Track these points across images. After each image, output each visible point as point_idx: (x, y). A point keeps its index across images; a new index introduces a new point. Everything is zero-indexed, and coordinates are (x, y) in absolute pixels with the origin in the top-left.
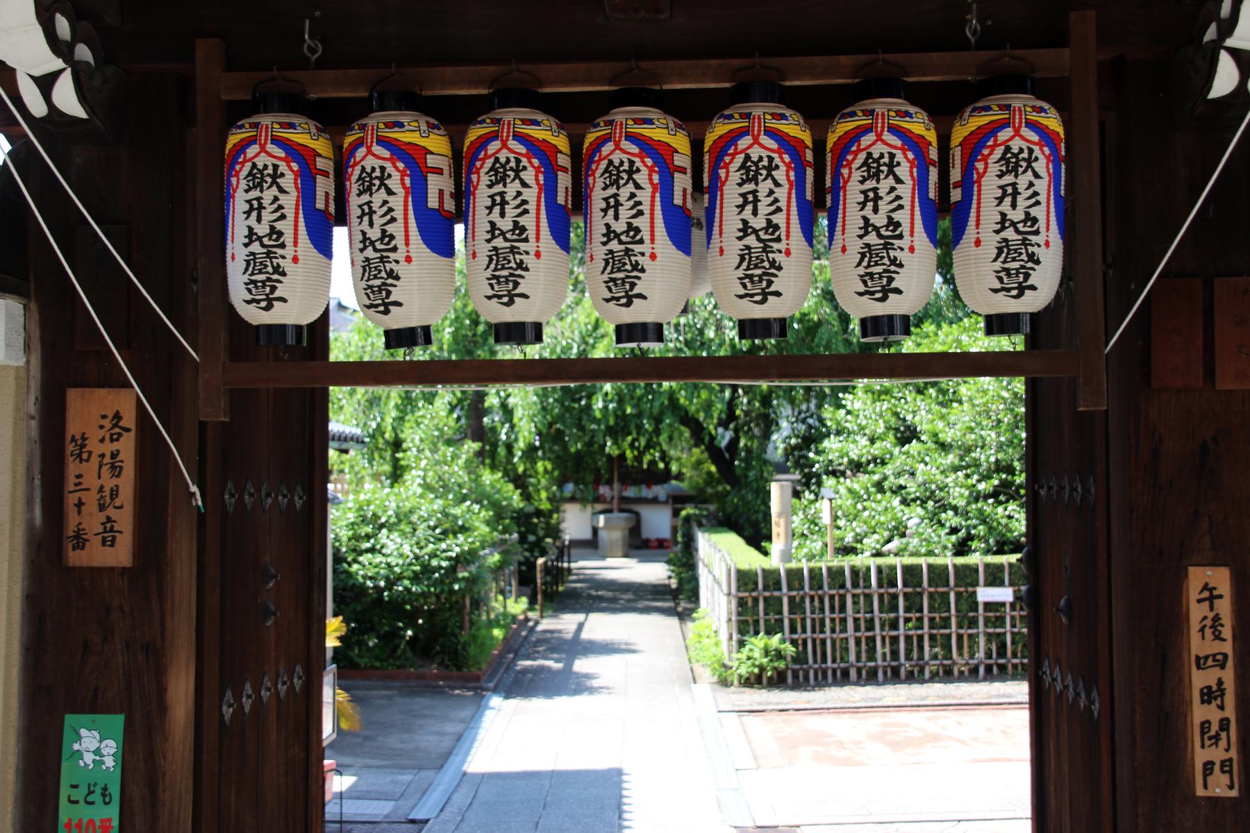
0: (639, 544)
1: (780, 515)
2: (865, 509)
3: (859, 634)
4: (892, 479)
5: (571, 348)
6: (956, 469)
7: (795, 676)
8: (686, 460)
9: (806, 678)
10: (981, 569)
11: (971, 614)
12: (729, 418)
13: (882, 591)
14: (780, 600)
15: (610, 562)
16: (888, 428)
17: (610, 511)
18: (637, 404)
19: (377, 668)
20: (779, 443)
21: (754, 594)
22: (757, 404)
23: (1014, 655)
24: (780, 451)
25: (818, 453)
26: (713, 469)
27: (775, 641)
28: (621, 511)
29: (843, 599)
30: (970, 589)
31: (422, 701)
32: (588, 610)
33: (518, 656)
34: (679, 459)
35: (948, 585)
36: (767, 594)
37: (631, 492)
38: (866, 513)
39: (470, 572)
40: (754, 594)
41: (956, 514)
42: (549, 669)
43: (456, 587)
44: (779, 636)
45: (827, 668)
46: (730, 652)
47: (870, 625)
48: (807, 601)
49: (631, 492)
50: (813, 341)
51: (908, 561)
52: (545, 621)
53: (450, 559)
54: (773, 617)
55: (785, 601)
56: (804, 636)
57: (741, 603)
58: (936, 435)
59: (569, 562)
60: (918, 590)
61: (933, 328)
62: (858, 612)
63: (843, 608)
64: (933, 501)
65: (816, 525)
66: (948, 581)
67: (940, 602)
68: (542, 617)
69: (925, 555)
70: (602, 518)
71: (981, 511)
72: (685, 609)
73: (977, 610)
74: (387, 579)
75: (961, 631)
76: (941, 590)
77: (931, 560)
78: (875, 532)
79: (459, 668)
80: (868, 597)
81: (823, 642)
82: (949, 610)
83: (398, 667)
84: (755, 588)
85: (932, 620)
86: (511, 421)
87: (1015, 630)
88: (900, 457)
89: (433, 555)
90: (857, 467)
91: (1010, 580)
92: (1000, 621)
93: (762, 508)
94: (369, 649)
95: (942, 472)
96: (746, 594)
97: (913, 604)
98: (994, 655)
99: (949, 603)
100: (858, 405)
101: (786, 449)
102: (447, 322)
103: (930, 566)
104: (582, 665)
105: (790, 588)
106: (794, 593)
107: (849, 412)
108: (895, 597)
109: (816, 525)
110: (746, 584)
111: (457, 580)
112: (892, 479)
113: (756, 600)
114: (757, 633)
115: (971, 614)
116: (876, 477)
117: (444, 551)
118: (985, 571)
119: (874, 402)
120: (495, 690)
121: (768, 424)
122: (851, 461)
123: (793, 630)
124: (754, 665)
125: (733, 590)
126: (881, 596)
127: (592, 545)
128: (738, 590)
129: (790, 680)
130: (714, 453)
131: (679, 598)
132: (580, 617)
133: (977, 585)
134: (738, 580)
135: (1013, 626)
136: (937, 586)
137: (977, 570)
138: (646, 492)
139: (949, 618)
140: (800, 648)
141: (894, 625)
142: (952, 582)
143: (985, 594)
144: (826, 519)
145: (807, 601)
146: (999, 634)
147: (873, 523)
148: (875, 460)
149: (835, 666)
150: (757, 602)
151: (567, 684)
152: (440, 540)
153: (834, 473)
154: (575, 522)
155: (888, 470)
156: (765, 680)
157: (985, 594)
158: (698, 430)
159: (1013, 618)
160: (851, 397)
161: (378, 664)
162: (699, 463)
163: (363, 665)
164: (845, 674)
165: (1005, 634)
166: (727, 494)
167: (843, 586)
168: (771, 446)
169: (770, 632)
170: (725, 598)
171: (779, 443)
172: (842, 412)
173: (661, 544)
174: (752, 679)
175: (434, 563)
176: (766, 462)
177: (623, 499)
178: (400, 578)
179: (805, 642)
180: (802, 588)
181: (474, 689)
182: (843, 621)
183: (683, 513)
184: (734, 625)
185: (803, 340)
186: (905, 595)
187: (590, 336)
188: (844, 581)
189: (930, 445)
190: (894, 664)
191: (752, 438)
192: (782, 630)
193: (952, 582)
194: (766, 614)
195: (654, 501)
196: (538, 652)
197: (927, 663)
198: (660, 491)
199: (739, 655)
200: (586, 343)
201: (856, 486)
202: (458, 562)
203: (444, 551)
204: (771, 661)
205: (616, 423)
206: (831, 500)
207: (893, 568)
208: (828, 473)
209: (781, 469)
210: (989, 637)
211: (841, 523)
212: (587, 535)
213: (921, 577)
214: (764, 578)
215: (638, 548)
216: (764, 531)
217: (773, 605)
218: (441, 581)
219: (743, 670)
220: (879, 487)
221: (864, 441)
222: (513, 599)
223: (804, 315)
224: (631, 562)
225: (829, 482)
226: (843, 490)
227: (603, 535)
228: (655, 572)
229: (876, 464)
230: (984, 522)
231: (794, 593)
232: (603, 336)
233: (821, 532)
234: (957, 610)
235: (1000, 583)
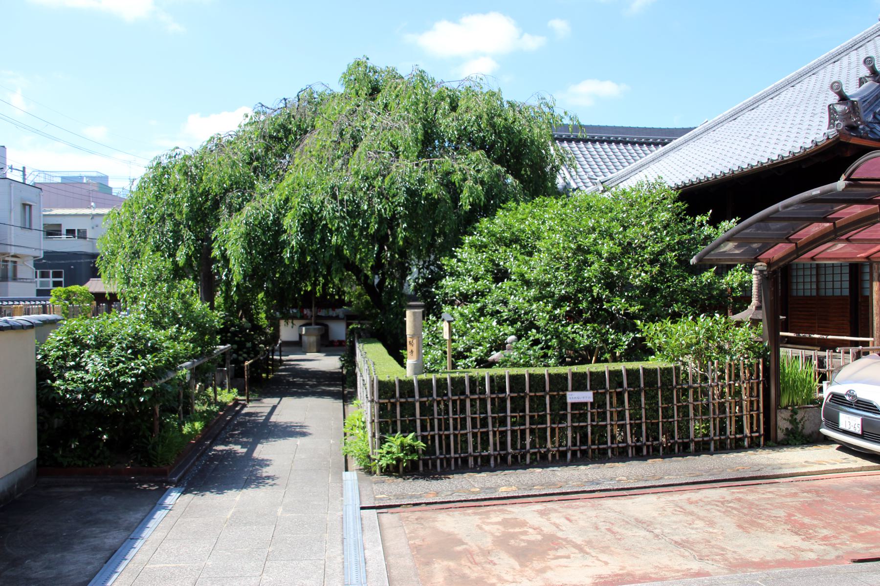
0: (326, 345)
1: (413, 337)
2: (472, 327)
4: (490, 306)
5: (269, 216)
6: (537, 299)
7: (425, 464)
8: (353, 291)
9: (434, 466)
10: (569, 377)
11: (562, 412)
12: (378, 266)
13: (494, 396)
14: (413, 405)
15: (309, 356)
16: (487, 271)
17: (310, 324)
18: (313, 253)
19: (79, 466)
20: (410, 283)
21: (392, 400)
22: (397, 256)
23: (593, 443)
24: (412, 287)
25: (437, 288)
26: (368, 298)
27: (409, 439)
28: (317, 324)
29: (463, 402)
30: (561, 393)
32: (281, 395)
33: (215, 442)
34: (349, 293)
35: (544, 390)
36: (403, 400)
37: (323, 313)
38: (474, 331)
39: (155, 387)
40: (392, 400)
41: (538, 332)
42: (235, 453)
43: (142, 400)
44: (411, 435)
45: (451, 458)
46: (373, 448)
47: (484, 423)
49: (323, 313)
50: (434, 213)
51: (515, 371)
52: (250, 404)
53: (136, 376)
54: (407, 419)
55: (417, 405)
56: (432, 433)
57: (382, 408)
58: (522, 275)
59: (280, 356)
60: (522, 394)
61: (514, 204)
62: (475, 413)
63: (463, 410)
64: (524, 325)
68: (249, 401)
69: (524, 366)
70: (304, 328)
71: (556, 329)
72: (349, 392)
73: (566, 409)
74: (84, 392)
75: (554, 426)
76: (582, 424)
77: (531, 370)
78: (480, 345)
79: (150, 465)
80: (483, 401)
81: (448, 437)
82: (545, 410)
83: (97, 465)
84: (394, 396)
85: (531, 417)
86: (227, 267)
87: (594, 423)
88: (497, 292)
89: (121, 373)
90: (465, 298)
91: (591, 385)
92: (582, 417)
93: (400, 325)
94: (72, 450)
95: (528, 301)
96: (387, 401)
97: (518, 406)
98: (578, 444)
99: (545, 404)
100: (465, 255)
101: (415, 286)
102: (185, 199)
103: (530, 375)
104: (263, 451)
105: (421, 396)
106: (425, 399)
107: (459, 261)
108: (503, 400)
109: (438, 338)
110: (386, 393)
111: (143, 394)
112: (490, 306)
113: (394, 405)
114: (395, 432)
115: (562, 412)
116: (479, 305)
117: (132, 369)
118: (572, 379)
119: (477, 253)
120: (177, 485)
121: (405, 271)
122: (461, 294)
123: (424, 428)
124: (392, 459)
125: (376, 399)
126: (493, 400)
127: (297, 345)
128: (380, 398)
129: (421, 469)
130: (369, 288)
131: (342, 385)
132: (275, 401)
133: (567, 390)
134: (379, 390)
135: (593, 420)
136: (536, 391)
137: (566, 378)
138: (332, 313)
139: (545, 416)
140: (429, 442)
141: (503, 422)
142: (547, 388)
143: (573, 397)
144: (446, 336)
146: (582, 427)
147: (478, 337)
148: (477, 293)
149: (457, 456)
150: (396, 407)
151: (239, 474)
152: (130, 359)
153: (452, 303)
154: (288, 332)
155: (489, 299)
156: (401, 469)
157: (573, 397)
158: (357, 271)
159: (592, 414)
160: (460, 250)
161: (80, 463)
162: (360, 295)
164: (465, 461)
165: (587, 426)
167: (463, 393)
168: (406, 284)
169: (405, 431)
170: (369, 404)
171: (410, 283)
173: (341, 343)
175: (122, 379)
176: (403, 295)
177: (318, 317)
178: (95, 391)
179: (433, 437)
180: (432, 395)
182: (464, 420)
183: (351, 327)
184: (376, 425)
185: (428, 212)
186: (512, 398)
187: (282, 208)
189: (519, 282)
190: (502, 452)
191: (393, 280)
192: (415, 430)
193: (547, 388)
194: (402, 416)
195: (337, 318)
196: (232, 436)
197: (528, 451)
198: (339, 312)
199: (381, 451)
200: (280, 213)
201: (466, 311)
202: (143, 378)
203: (132, 369)
204: (406, 454)
205: (299, 267)
206: (449, 322)
207: (502, 378)
208: (445, 302)
209: (413, 298)
210: (574, 429)
211: (456, 337)
212: (296, 338)
213: (524, 385)
214: (400, 387)
215: (327, 346)
216: (402, 341)
217: (407, 409)
218: (129, 395)
219: (384, 463)
220: (481, 310)
221: (470, 280)
222: (227, 390)
223: (428, 195)
224: (320, 356)
225: (447, 309)
226: (457, 315)
227: (305, 338)
228: (330, 363)
229: (478, 296)
230: (557, 337)
231: (425, 399)
232: (291, 208)
233: (442, 343)
235: (584, 389)
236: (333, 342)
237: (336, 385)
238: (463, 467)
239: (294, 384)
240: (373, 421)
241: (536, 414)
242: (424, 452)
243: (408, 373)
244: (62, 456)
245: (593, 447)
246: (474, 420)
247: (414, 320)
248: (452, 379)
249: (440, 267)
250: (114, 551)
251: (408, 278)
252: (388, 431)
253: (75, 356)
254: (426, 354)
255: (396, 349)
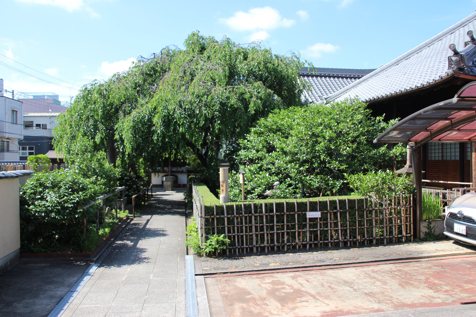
0: (176, 187)
1: (223, 182)
2: (255, 177)
3: (257, 233)
4: (265, 166)
5: (145, 117)
6: (290, 162)
7: (230, 251)
8: (191, 157)
9: (235, 252)
10: (308, 204)
12: (204, 144)
13: (267, 214)
14: (223, 219)
15: (167, 192)
16: (263, 147)
17: (168, 175)
18: (170, 137)
20: (222, 153)
21: (212, 217)
22: (215, 138)
23: (321, 240)
24: (223, 155)
25: (236, 156)
26: (199, 161)
27: (221, 237)
28: (171, 175)
29: (250, 218)
30: (304, 213)
31: (58, 270)
32: (152, 213)
33: (116, 239)
34: (189, 158)
35: (294, 211)
36: (218, 216)
37: (174, 169)
38: (256, 179)
39: (84, 209)
40: (212, 217)
41: (291, 180)
42: (127, 245)
43: (77, 216)
44: (223, 235)
45: (244, 248)
46: (202, 242)
47: (262, 229)
48: (235, 219)
49: (174, 169)
50: (235, 115)
51: (279, 201)
52: (135, 219)
53: (73, 203)
54: (220, 226)
55: (226, 219)
56: (234, 234)
57: (207, 220)
58: (282, 149)
59: (152, 192)
60: (282, 213)
61: (278, 111)
62: (257, 224)
63: (251, 222)
64: (283, 176)
65: (237, 183)
66: (294, 209)
67: (291, 218)
68: (134, 217)
70: (164, 178)
71: (301, 178)
72: (189, 212)
73: (306, 221)
74: (45, 212)
75: (299, 230)
77: (287, 200)
78: (260, 187)
79: (81, 251)
80: (261, 217)
81: (242, 236)
82: (295, 222)
83: (52, 251)
84: (213, 214)
85: (287, 226)
86: (123, 144)
87: (321, 229)
88: (269, 158)
89: (66, 202)
90: (252, 161)
91: (320, 208)
92: (315, 225)
93: (217, 176)
94: (39, 244)
95: (286, 163)
96: (209, 217)
97: (280, 219)
98: (313, 240)
99: (295, 219)
100: (251, 138)
101: (224, 155)
102: (100, 108)
103: (287, 203)
104: (142, 244)
105: (228, 214)
106: (230, 216)
107: (248, 141)
108: (272, 217)
109: (237, 183)
110: (209, 212)
111: (77, 213)
112: (265, 166)
113: (213, 219)
114: (214, 233)
116: (259, 165)
117: (72, 200)
120: (96, 262)
121: (219, 147)
122: (249, 159)
123: (229, 232)
124: (212, 248)
125: (203, 216)
126: (266, 216)
127: (161, 187)
128: (205, 215)
130: (199, 156)
131: (185, 208)
132: (149, 217)
133: (307, 211)
134: (205, 211)
135: (321, 227)
136: (290, 212)
137: (306, 205)
138: (179, 169)
139: (295, 225)
140: (232, 239)
141: (272, 228)
142: (296, 210)
143: (310, 215)
144: (241, 182)
145: (235, 219)
146: (315, 231)
147: (259, 182)
148: (258, 159)
149: (247, 246)
150: (214, 220)
151: (129, 256)
152: (71, 194)
153: (244, 164)
154: (156, 179)
155: (264, 162)
156: (217, 254)
157: (310, 215)
158: (193, 146)
159: (320, 224)
160: (249, 135)
161: (43, 250)
162: (195, 160)
163: (35, 251)
166: (204, 170)
167: (251, 213)
168: (220, 154)
169: (219, 233)
170: (200, 218)
171: (222, 153)
172: (246, 141)
173: (184, 186)
174: (212, 253)
175: (66, 205)
176: (218, 159)
178: (52, 211)
179: (234, 236)
180: (233, 214)
181: (86, 261)
182: (251, 227)
183: (190, 177)
184: (203, 230)
185: (231, 114)
186: (277, 215)
187: (153, 113)
188: (251, 210)
189: (281, 153)
192: (224, 233)
193: (296, 210)
194: (217, 225)
195: (182, 172)
196: (126, 236)
197: (286, 244)
198: (184, 169)
199: (206, 244)
200: (151, 115)
201: (252, 168)
202: (77, 205)
203: (72, 200)
204: (220, 246)
205: (162, 145)
206: (243, 174)
207: (272, 204)
208: (241, 164)
209: (223, 161)
210: (311, 232)
211: (247, 183)
212: (160, 183)
213: (284, 208)
215: (177, 187)
216: (217, 184)
217: (220, 221)
218: (70, 214)
219: (207, 250)
220: (260, 168)
221: (254, 152)
222: (123, 211)
223: (232, 105)
224: (173, 192)
225: (242, 167)
226: (247, 170)
227: (165, 183)
228: (179, 196)
229: (259, 160)
230: (302, 182)
231: (230, 216)
232: (157, 113)
233: (239, 185)
234: (298, 222)
236: (180, 185)
237: (182, 208)
238: (250, 252)
239: (159, 208)
240: (202, 228)
241: (290, 224)
242: (229, 245)
243: (221, 202)
244: (34, 247)
245: (321, 242)
246: (256, 227)
247: (224, 173)
248: (245, 205)
249: (238, 145)
250: (61, 298)
251: (221, 150)
252: (210, 233)
253: (40, 192)
254: (231, 191)
255: (214, 189)
